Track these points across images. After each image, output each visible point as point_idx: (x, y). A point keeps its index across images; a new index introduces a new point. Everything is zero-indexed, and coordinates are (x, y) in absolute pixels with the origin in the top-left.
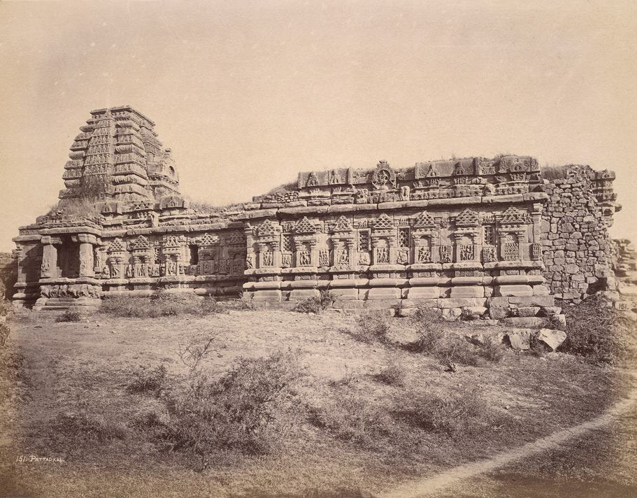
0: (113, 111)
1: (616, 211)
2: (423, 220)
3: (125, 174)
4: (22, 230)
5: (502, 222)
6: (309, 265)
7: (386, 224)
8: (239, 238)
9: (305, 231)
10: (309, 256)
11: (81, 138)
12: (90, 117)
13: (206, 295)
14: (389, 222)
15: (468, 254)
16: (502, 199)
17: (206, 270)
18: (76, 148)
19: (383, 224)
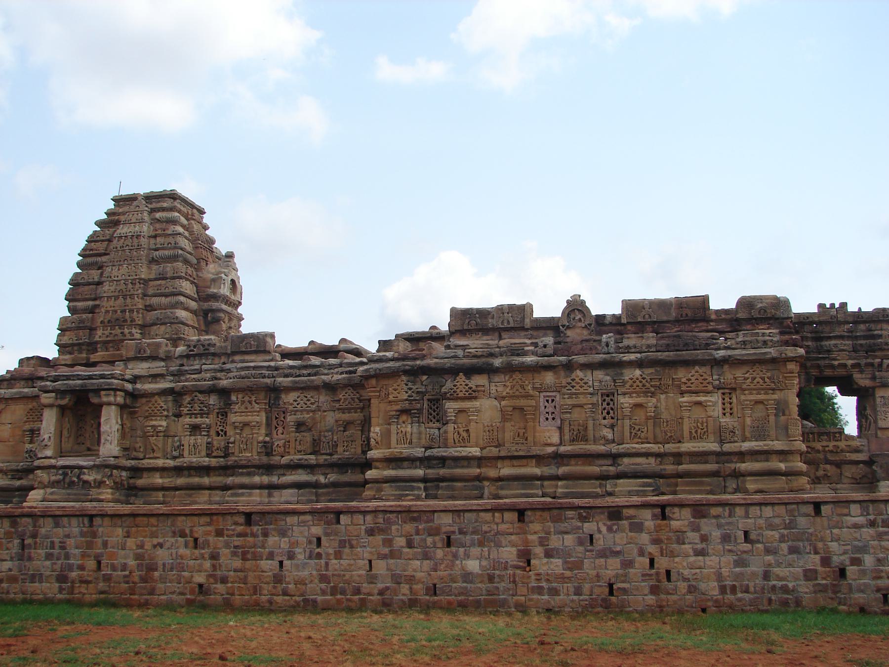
2: (634, 382)
3: (166, 296)
5: (744, 386)
6: (468, 444)
7: (581, 387)
8: (763, 379)
9: (461, 395)
10: (467, 431)
11: (95, 239)
13: (822, 332)
14: (585, 383)
15: (699, 431)
16: (743, 355)
17: (299, 448)
18: (88, 253)
19: (577, 387)
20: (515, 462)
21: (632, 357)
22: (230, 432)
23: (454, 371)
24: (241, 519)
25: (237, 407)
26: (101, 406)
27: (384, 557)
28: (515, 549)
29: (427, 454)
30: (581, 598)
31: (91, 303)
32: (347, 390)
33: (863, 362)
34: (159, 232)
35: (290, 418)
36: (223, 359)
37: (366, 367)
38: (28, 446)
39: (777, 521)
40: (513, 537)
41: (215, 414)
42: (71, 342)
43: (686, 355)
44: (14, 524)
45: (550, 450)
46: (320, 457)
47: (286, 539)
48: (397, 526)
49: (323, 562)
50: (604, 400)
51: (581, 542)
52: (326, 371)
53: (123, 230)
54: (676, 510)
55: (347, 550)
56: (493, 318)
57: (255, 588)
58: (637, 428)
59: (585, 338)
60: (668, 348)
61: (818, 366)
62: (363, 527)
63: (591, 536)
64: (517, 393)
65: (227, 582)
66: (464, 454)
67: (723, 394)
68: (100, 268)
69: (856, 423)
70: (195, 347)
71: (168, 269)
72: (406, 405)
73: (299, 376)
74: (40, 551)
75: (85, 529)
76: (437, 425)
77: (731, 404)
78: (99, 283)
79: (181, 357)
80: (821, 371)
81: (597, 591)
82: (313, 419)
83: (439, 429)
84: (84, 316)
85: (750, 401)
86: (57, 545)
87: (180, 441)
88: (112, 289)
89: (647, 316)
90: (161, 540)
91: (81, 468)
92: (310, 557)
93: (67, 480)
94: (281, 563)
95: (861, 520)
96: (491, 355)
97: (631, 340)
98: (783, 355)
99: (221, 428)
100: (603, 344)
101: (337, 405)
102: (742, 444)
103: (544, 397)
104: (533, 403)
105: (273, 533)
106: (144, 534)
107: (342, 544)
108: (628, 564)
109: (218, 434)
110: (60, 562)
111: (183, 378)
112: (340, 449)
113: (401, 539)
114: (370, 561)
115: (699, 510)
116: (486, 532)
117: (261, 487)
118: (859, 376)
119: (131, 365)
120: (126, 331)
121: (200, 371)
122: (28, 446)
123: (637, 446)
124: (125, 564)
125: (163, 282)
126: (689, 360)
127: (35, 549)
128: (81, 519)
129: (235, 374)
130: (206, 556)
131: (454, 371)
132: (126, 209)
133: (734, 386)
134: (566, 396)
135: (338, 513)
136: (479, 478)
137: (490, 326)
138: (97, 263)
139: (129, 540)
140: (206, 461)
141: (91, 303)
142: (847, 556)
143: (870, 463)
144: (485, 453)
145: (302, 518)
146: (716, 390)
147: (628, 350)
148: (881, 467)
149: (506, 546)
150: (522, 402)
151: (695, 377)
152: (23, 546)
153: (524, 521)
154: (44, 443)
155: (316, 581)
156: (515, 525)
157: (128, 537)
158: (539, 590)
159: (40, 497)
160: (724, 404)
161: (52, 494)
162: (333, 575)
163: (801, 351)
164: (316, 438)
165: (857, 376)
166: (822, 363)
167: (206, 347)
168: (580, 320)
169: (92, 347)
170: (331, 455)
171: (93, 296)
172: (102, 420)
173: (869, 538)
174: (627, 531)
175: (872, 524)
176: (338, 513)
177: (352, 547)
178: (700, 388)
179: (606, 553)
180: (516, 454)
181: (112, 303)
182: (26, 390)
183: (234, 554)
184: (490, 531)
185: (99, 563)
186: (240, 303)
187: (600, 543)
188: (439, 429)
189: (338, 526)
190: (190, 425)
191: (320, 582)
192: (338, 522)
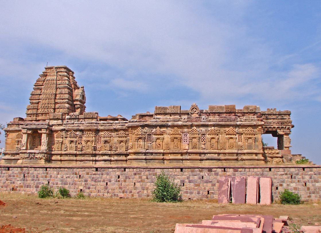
0: (56, 68)
1: (292, 128)
2: (212, 131)
3: (62, 99)
4: (8, 125)
7: (195, 132)
9: (158, 133)
12: (44, 70)
14: (197, 131)
17: (105, 149)
18: (37, 85)
20: (174, 155)
21: (212, 123)
22: (83, 143)
23: (155, 126)
24: (95, 169)
25: (86, 135)
26: (41, 134)
27: (140, 182)
28: (179, 180)
29: (147, 152)
30: (199, 195)
31: (37, 101)
32: (121, 131)
33: (280, 127)
34: (60, 79)
35: (103, 139)
36: (81, 120)
37: (128, 124)
38: (17, 146)
39: (258, 173)
40: (179, 176)
41: (78, 137)
42: (31, 113)
43: (228, 123)
44: (22, 170)
45: (185, 151)
46: (112, 152)
47: (108, 176)
48: (143, 172)
49: (120, 183)
50: (202, 136)
51: (199, 178)
52: (114, 125)
53: (48, 78)
54: (228, 169)
55: (128, 180)
56: (168, 110)
57: (99, 190)
58: (212, 145)
59: (197, 117)
60: (222, 121)
61: (267, 128)
62: (133, 173)
63: (203, 176)
64: (176, 133)
65: (90, 189)
66: (159, 152)
67: (239, 135)
68: (41, 90)
69: (277, 145)
70: (72, 116)
71: (63, 91)
72: (141, 136)
73: (106, 126)
74: (30, 178)
75: (45, 172)
76: (150, 142)
77: (241, 138)
78: (40, 95)
79: (68, 119)
80: (268, 129)
81: (204, 193)
82: (110, 140)
83: (151, 144)
84: (35, 105)
85: (247, 137)
86: (35, 176)
87: (66, 145)
88: (45, 96)
89: (216, 111)
90: (69, 176)
91: (35, 153)
92: (116, 182)
93: (30, 157)
94: (107, 183)
95: (283, 173)
96: (168, 121)
97: (211, 118)
98: (258, 124)
99: (80, 142)
100: (203, 119)
101: (118, 135)
102: (244, 151)
103: (184, 135)
104: (180, 136)
105: (105, 174)
106: (63, 174)
107: (126, 177)
108: (214, 185)
109: (79, 144)
110: (36, 182)
111: (68, 126)
112: (118, 149)
113: (144, 176)
114: (135, 183)
115: (235, 169)
116: (171, 175)
117: (93, 161)
118: (279, 131)
119: (51, 121)
120: (49, 110)
121: (73, 124)
122: (17, 146)
123: (212, 150)
124: (57, 183)
125: (61, 95)
126: (229, 125)
127: (28, 177)
128: (43, 169)
129: (85, 125)
130: (83, 181)
131: (155, 126)
132: (49, 71)
133: (243, 133)
134: (191, 135)
135: (125, 168)
136: (163, 159)
137: (168, 112)
138: (40, 88)
139: (58, 175)
140: (75, 152)
141: (37, 101)
142: (278, 183)
143: (282, 157)
144: (165, 151)
145: (114, 169)
146: (237, 134)
147: (210, 121)
148: (285, 158)
149: (177, 179)
150: (177, 136)
151: (230, 130)
152: (24, 177)
153: (182, 171)
154: (23, 145)
155: (118, 189)
156: (180, 173)
157: (58, 174)
158: (187, 192)
159: (21, 162)
160: (239, 138)
161: (25, 161)
162: (123, 187)
163: (263, 123)
164: (111, 146)
165: (278, 131)
166: (268, 126)
167: (76, 116)
168: (195, 111)
169: (37, 115)
170: (115, 151)
171: (38, 99)
172: (42, 138)
173: (285, 178)
174: (214, 175)
175: (286, 174)
176: (125, 168)
177: (129, 178)
178: (232, 133)
179: (207, 182)
180: (175, 152)
181: (44, 101)
182: (17, 128)
183: (92, 180)
184: (172, 174)
185: (49, 182)
186: (85, 103)
187: (205, 178)
188: (151, 144)
189: (125, 172)
190: (70, 141)
191: (119, 189)
192: (125, 171)
